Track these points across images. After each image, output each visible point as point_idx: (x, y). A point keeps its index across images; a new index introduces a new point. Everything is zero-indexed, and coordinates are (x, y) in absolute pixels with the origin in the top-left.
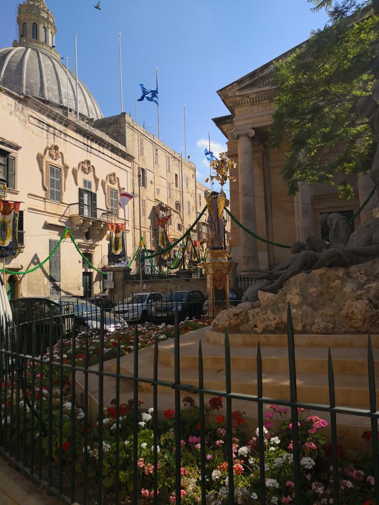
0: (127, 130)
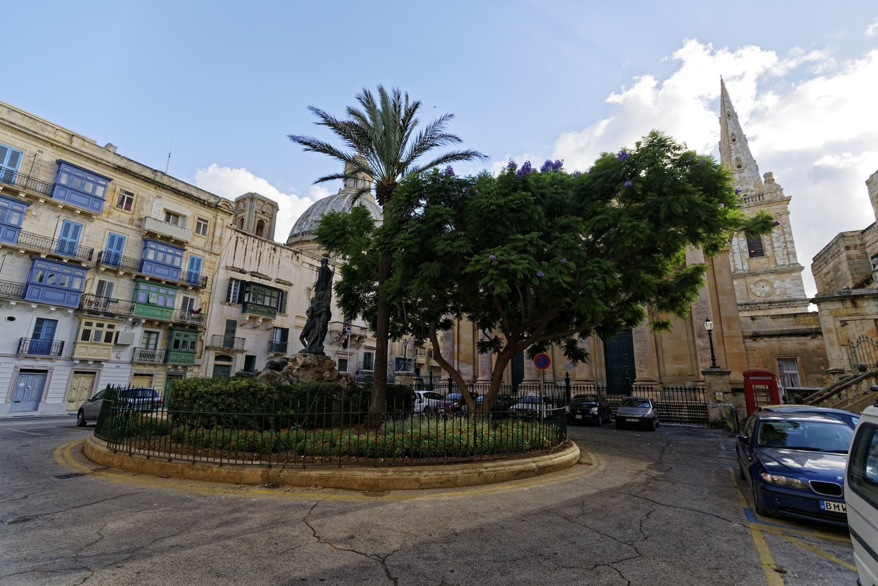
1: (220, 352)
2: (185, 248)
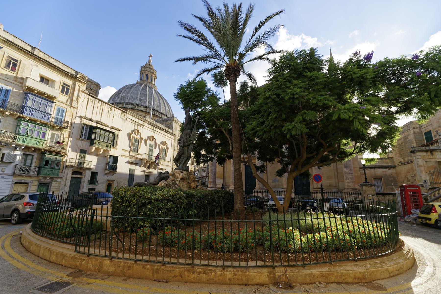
0: (174, 124)
1: (75, 170)
2: (54, 101)
